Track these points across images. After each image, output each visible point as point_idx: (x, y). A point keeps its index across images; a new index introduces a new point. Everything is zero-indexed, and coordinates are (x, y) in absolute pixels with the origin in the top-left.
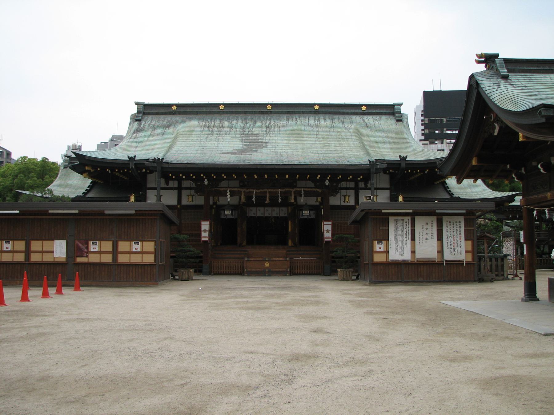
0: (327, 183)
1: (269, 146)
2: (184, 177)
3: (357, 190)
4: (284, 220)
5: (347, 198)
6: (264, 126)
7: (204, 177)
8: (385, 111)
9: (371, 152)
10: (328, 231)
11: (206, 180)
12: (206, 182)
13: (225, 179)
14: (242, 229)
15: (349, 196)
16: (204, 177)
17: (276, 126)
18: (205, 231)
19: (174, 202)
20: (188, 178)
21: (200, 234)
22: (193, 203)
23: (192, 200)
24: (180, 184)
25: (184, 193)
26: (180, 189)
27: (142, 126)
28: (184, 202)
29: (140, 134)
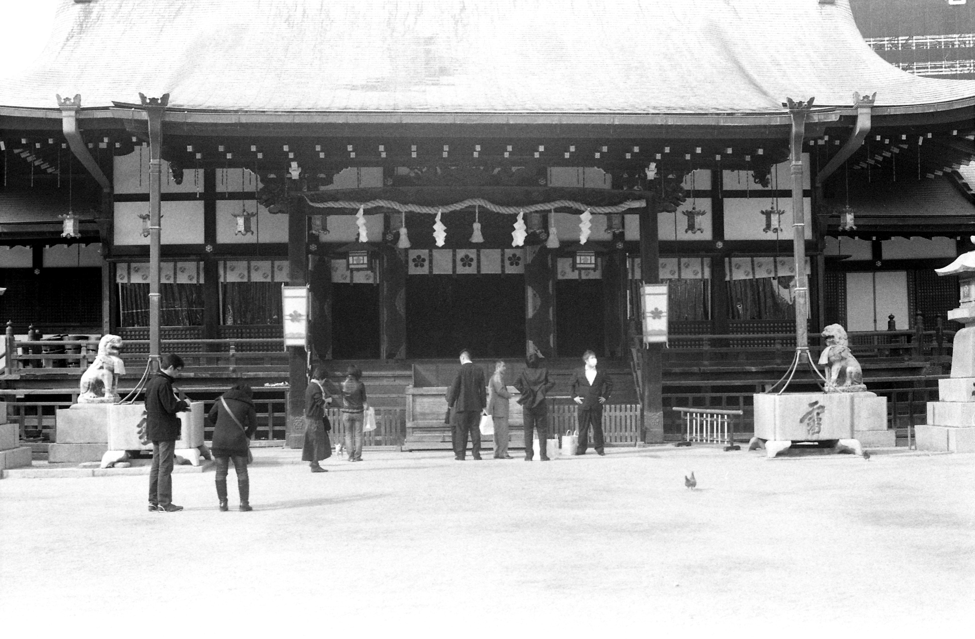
0: (651, 173)
3: (718, 196)
5: (774, 219)
7: (291, 156)
10: (657, 314)
11: (294, 165)
12: (295, 172)
14: (393, 309)
15: (780, 213)
16: (291, 156)
18: (295, 317)
19: (195, 236)
20: (243, 160)
22: (249, 239)
23: (248, 229)
25: (223, 208)
26: (210, 198)
28: (225, 236)
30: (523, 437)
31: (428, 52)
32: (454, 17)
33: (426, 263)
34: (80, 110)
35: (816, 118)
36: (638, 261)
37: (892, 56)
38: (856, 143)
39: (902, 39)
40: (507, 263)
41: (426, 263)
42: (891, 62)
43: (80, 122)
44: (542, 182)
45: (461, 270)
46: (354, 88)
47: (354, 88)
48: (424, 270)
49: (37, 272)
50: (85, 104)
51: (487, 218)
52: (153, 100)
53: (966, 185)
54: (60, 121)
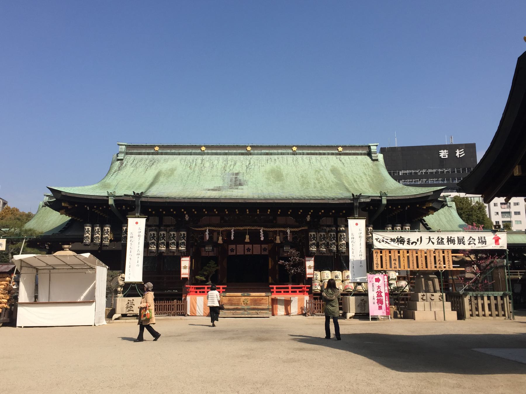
0: (308, 218)
1: (250, 183)
2: (154, 212)
4: (266, 257)
6: (244, 166)
7: (185, 213)
8: (360, 152)
9: (350, 189)
11: (187, 216)
12: (187, 218)
13: (206, 215)
16: (185, 213)
17: (256, 166)
21: (305, 271)
24: (161, 221)
27: (124, 165)
29: (122, 173)
30: (193, 297)
31: (236, 178)
32: (246, 166)
33: (235, 251)
34: (114, 196)
35: (362, 200)
36: (107, 228)
37: (397, 178)
38: (382, 209)
39: (424, 171)
40: (262, 250)
41: (235, 251)
42: (396, 180)
43: (115, 201)
44: (274, 222)
45: (246, 253)
46: (209, 190)
47: (209, 190)
48: (234, 253)
49: (99, 252)
50: (117, 194)
51: (251, 233)
52: (138, 194)
53: (427, 224)
54: (108, 200)
